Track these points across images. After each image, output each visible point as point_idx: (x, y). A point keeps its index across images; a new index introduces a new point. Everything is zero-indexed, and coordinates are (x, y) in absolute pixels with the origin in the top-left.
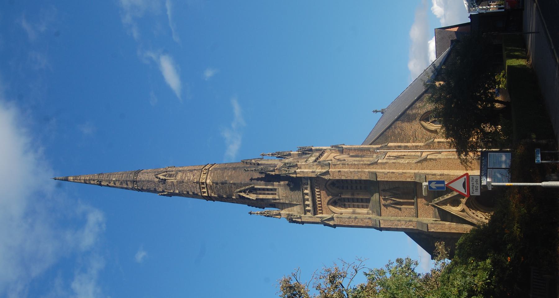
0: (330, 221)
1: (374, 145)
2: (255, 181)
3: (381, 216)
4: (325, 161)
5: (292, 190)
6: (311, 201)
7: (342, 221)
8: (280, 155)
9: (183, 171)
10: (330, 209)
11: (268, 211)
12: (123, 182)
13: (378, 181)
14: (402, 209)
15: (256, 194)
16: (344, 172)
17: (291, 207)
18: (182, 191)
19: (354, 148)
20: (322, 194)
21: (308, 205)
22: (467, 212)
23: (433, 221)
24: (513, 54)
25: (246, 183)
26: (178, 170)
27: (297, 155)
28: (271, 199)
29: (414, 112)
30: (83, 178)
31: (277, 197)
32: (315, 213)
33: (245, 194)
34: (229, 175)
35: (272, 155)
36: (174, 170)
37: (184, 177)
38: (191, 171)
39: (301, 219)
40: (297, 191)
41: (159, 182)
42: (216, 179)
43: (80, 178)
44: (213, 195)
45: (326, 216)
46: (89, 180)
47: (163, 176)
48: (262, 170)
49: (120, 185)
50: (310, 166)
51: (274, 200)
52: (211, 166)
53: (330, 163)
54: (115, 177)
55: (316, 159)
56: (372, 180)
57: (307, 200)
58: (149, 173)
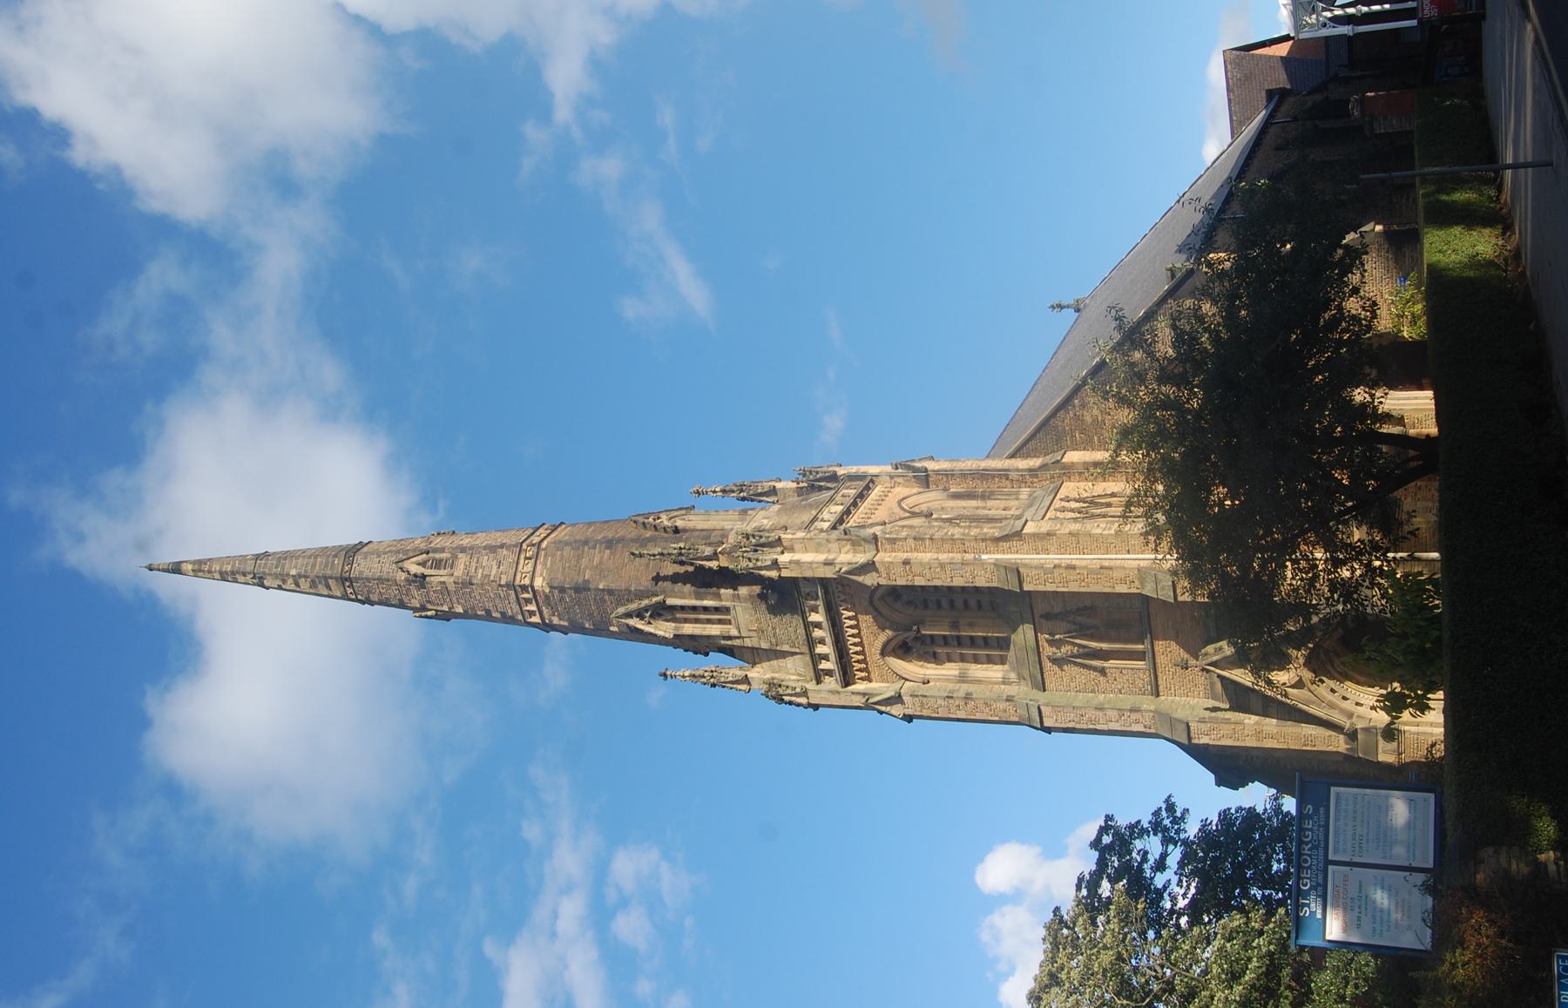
0: (891, 705)
1: (1027, 456)
2: (668, 584)
3: (1044, 690)
4: (863, 527)
5: (774, 610)
6: (832, 647)
7: (926, 707)
11: (714, 669)
15: (675, 620)
18: (473, 608)
19: (961, 470)
20: (863, 625)
21: (825, 657)
23: (1206, 709)
24: (1447, 198)
25: (642, 588)
28: (716, 636)
30: (218, 569)
31: (734, 632)
32: (847, 680)
35: (723, 491)
36: (447, 544)
37: (474, 567)
38: (492, 549)
39: (808, 699)
40: (788, 615)
41: (407, 580)
42: (559, 575)
43: (211, 567)
44: (556, 620)
45: (881, 688)
47: (419, 564)
48: (680, 554)
49: (311, 587)
52: (549, 531)
54: (295, 567)
55: (843, 515)
56: (1006, 588)
57: (820, 643)
58: (383, 556)
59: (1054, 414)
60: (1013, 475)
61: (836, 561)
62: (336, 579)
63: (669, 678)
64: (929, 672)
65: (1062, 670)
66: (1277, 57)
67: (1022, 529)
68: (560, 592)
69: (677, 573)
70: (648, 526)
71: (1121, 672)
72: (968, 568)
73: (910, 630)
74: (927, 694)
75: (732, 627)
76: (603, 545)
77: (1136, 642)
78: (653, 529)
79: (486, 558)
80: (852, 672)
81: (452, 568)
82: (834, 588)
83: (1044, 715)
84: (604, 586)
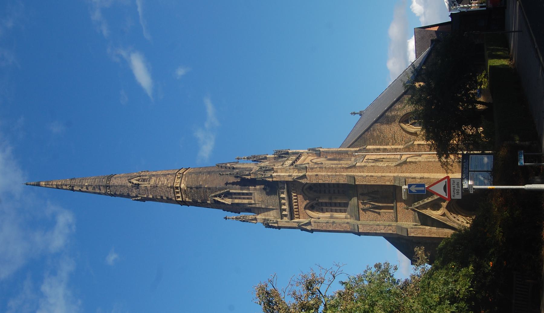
0: (307, 226)
2: (231, 185)
3: (359, 220)
4: (302, 164)
5: (268, 194)
6: (288, 206)
8: (255, 159)
10: (307, 214)
11: (244, 216)
13: (357, 185)
15: (231, 198)
16: (322, 175)
17: (267, 212)
18: (156, 196)
20: (299, 199)
21: (285, 210)
22: (448, 216)
23: (413, 225)
25: (221, 187)
27: (273, 158)
28: (246, 203)
29: (393, 113)
30: (55, 183)
31: (253, 202)
32: (292, 218)
35: (248, 158)
36: (147, 174)
38: (165, 175)
39: (278, 224)
40: (273, 195)
41: (132, 186)
43: (52, 183)
44: (187, 200)
46: (61, 185)
47: (137, 180)
49: (93, 190)
51: (250, 205)
52: (185, 170)
54: (87, 182)
55: (293, 163)
56: (350, 183)
58: (122, 178)
59: (364, 133)
60: (349, 153)
61: (292, 175)
62: (104, 186)
63: (228, 219)
64: (320, 215)
66: (434, 31)
67: (356, 165)
69: (234, 182)
70: (223, 167)
71: (385, 214)
72: (337, 177)
73: (315, 200)
74: (320, 222)
75: (252, 200)
76: (207, 173)
77: (391, 203)
78: (225, 168)
79: (162, 178)
81: (149, 182)
84: (207, 186)
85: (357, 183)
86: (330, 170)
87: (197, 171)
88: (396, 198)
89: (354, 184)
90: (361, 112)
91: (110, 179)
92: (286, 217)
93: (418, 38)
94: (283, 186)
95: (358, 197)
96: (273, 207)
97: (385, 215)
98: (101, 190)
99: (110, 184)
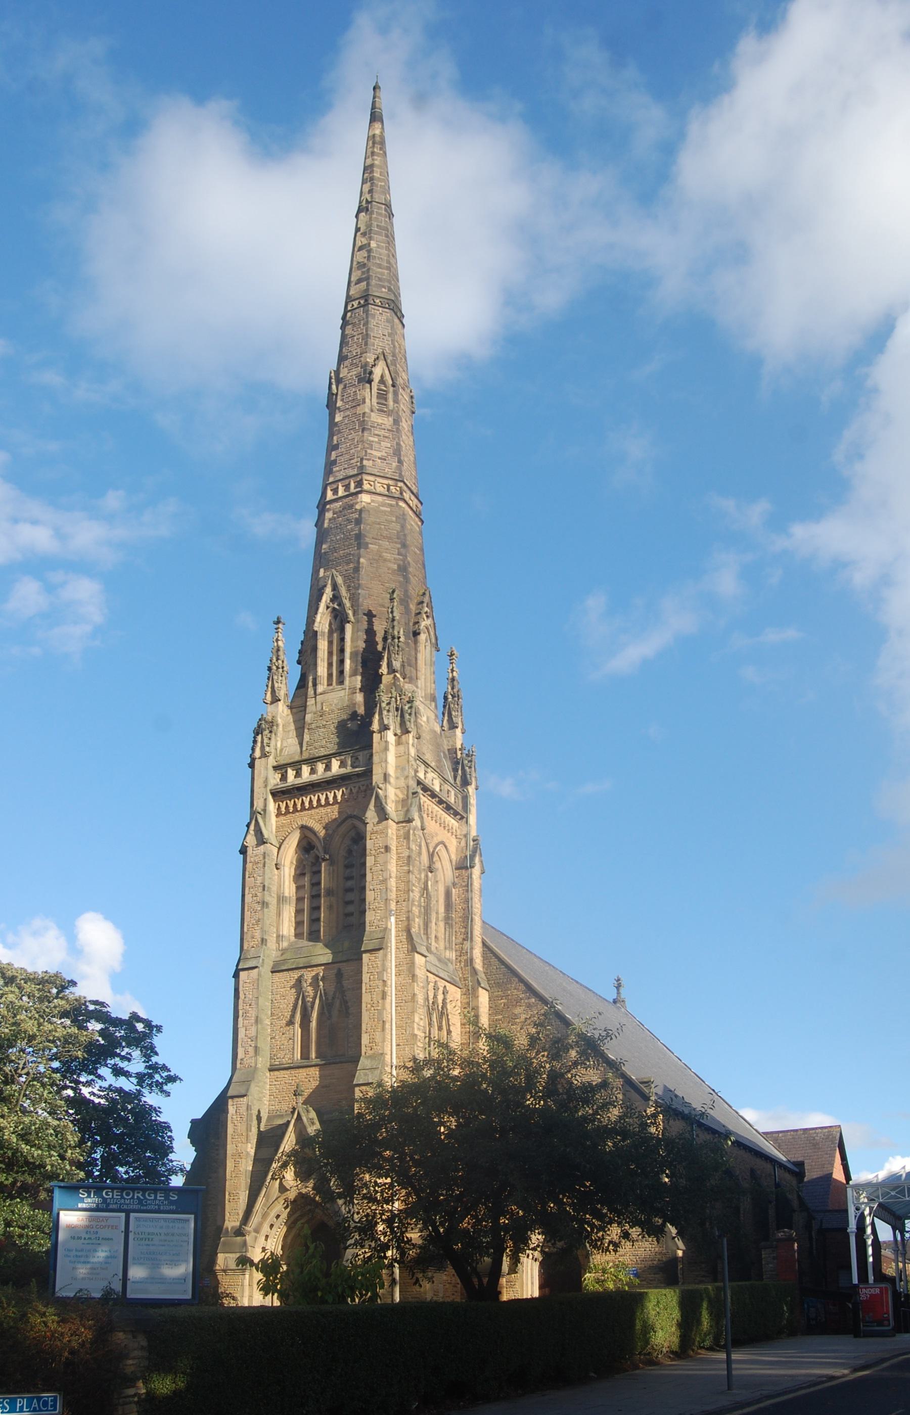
0: (256, 835)
1: (484, 957)
3: (272, 972)
4: (420, 810)
5: (341, 727)
8: (450, 700)
9: (398, 429)
10: (289, 833)
11: (285, 669)
12: (364, 270)
13: (360, 959)
14: (291, 1027)
15: (331, 632)
16: (386, 863)
17: (296, 729)
18: (339, 432)
19: (472, 899)
20: (329, 809)
21: (298, 774)
23: (259, 1111)
25: (361, 600)
26: (399, 416)
27: (452, 745)
30: (376, 162)
31: (320, 689)
32: (278, 794)
33: (328, 602)
34: (384, 554)
35: (453, 679)
36: (402, 406)
38: (397, 452)
39: (259, 758)
40: (337, 740)
42: (372, 519)
43: (378, 155)
44: (329, 515)
45: (271, 825)
46: (372, 179)
47: (382, 376)
49: (358, 263)
50: (405, 769)
51: (313, 682)
53: (414, 823)
54: (378, 247)
55: (430, 791)
56: (365, 939)
57: (312, 769)
58: (390, 339)
59: (522, 980)
61: (388, 784)
62: (367, 290)
63: (276, 626)
65: (291, 988)
66: (832, 1170)
67: (418, 953)
68: (356, 519)
69: (375, 635)
70: (420, 606)
71: (290, 1039)
73: (325, 853)
75: (325, 687)
76: (401, 563)
77: (317, 1052)
78: (417, 612)
79: (389, 445)
80: (286, 799)
82: (363, 783)
83: (250, 971)
84: (363, 563)
85: (365, 957)
86: (402, 886)
87: (409, 538)
88: (330, 1064)
89: (362, 949)
90: (623, 1001)
91: (387, 305)
92: (281, 780)
93: (814, 1135)
94: (361, 763)
95: (332, 963)
96: (308, 742)
97: (285, 1037)
98: (357, 286)
99: (373, 307)
